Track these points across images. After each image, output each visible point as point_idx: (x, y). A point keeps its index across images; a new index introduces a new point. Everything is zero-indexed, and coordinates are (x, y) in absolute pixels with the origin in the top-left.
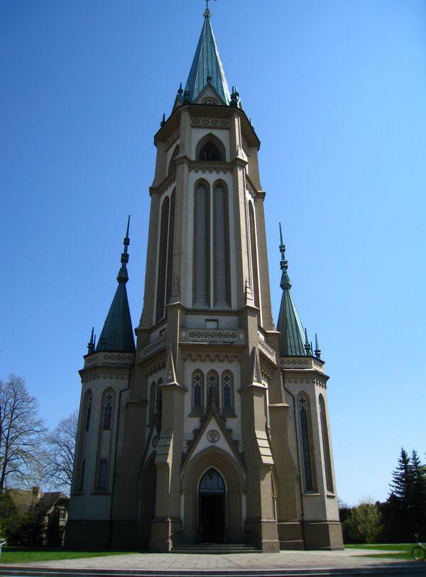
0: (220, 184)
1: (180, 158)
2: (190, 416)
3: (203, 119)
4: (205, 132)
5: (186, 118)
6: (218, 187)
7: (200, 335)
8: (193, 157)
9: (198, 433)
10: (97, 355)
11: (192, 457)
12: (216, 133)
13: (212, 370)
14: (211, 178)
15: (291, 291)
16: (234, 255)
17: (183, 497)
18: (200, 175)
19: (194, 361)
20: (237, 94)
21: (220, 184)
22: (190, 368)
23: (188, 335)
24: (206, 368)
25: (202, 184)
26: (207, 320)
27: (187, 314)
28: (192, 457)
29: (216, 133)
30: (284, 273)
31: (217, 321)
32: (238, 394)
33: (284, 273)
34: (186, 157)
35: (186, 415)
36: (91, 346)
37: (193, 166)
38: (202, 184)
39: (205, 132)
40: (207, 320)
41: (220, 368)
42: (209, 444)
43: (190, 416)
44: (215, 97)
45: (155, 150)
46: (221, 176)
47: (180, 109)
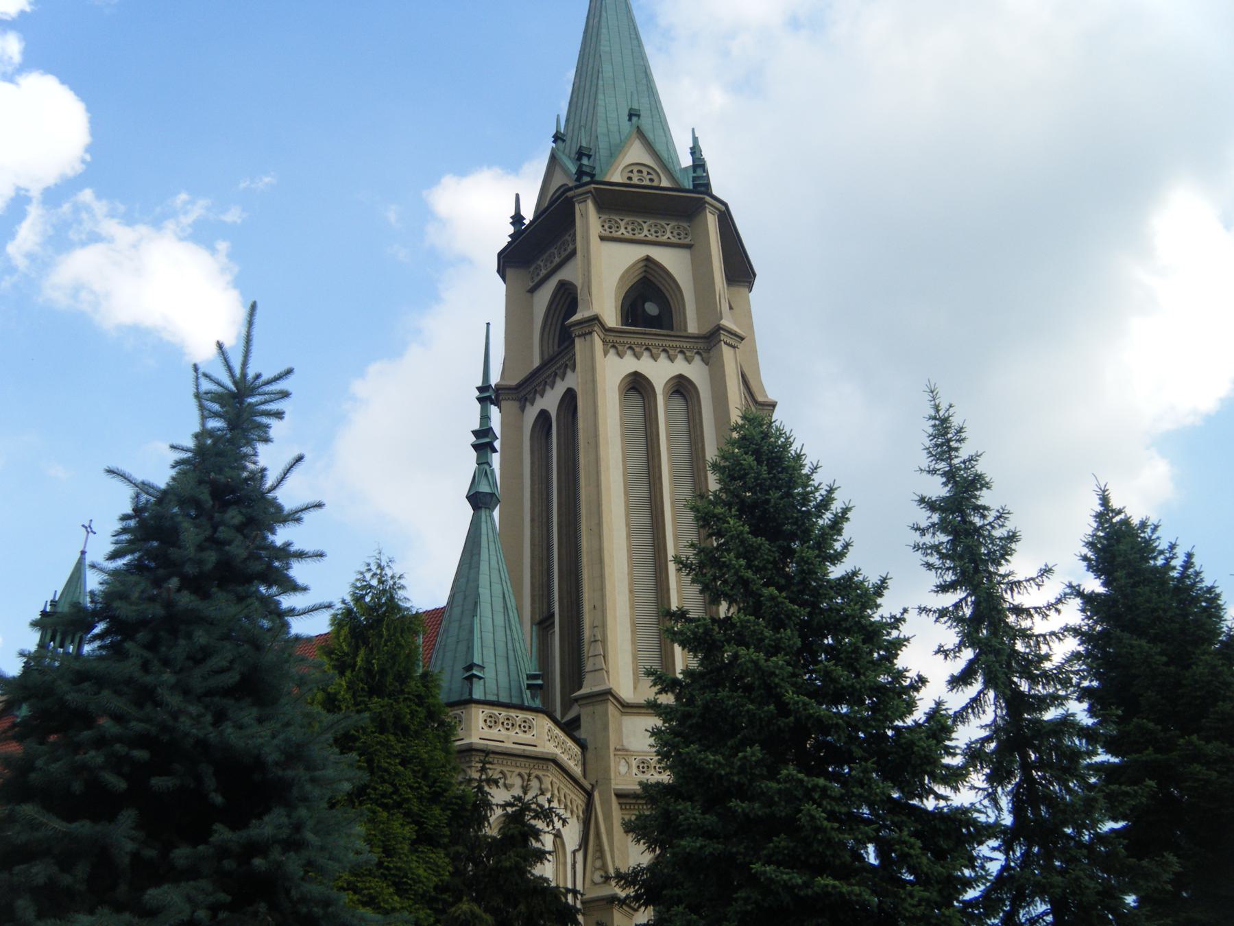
0: (681, 388)
1: (580, 323)
3: (627, 219)
5: (590, 220)
6: (631, 388)
8: (611, 318)
10: (529, 716)
12: (663, 256)
14: (660, 371)
16: (675, 578)
18: (629, 364)
20: (1070, 583)
21: (681, 388)
23: (635, 770)
25: (637, 385)
27: (623, 713)
29: (658, 254)
34: (596, 319)
37: (615, 342)
38: (637, 385)
45: (499, 287)
46: (680, 367)
47: (570, 194)
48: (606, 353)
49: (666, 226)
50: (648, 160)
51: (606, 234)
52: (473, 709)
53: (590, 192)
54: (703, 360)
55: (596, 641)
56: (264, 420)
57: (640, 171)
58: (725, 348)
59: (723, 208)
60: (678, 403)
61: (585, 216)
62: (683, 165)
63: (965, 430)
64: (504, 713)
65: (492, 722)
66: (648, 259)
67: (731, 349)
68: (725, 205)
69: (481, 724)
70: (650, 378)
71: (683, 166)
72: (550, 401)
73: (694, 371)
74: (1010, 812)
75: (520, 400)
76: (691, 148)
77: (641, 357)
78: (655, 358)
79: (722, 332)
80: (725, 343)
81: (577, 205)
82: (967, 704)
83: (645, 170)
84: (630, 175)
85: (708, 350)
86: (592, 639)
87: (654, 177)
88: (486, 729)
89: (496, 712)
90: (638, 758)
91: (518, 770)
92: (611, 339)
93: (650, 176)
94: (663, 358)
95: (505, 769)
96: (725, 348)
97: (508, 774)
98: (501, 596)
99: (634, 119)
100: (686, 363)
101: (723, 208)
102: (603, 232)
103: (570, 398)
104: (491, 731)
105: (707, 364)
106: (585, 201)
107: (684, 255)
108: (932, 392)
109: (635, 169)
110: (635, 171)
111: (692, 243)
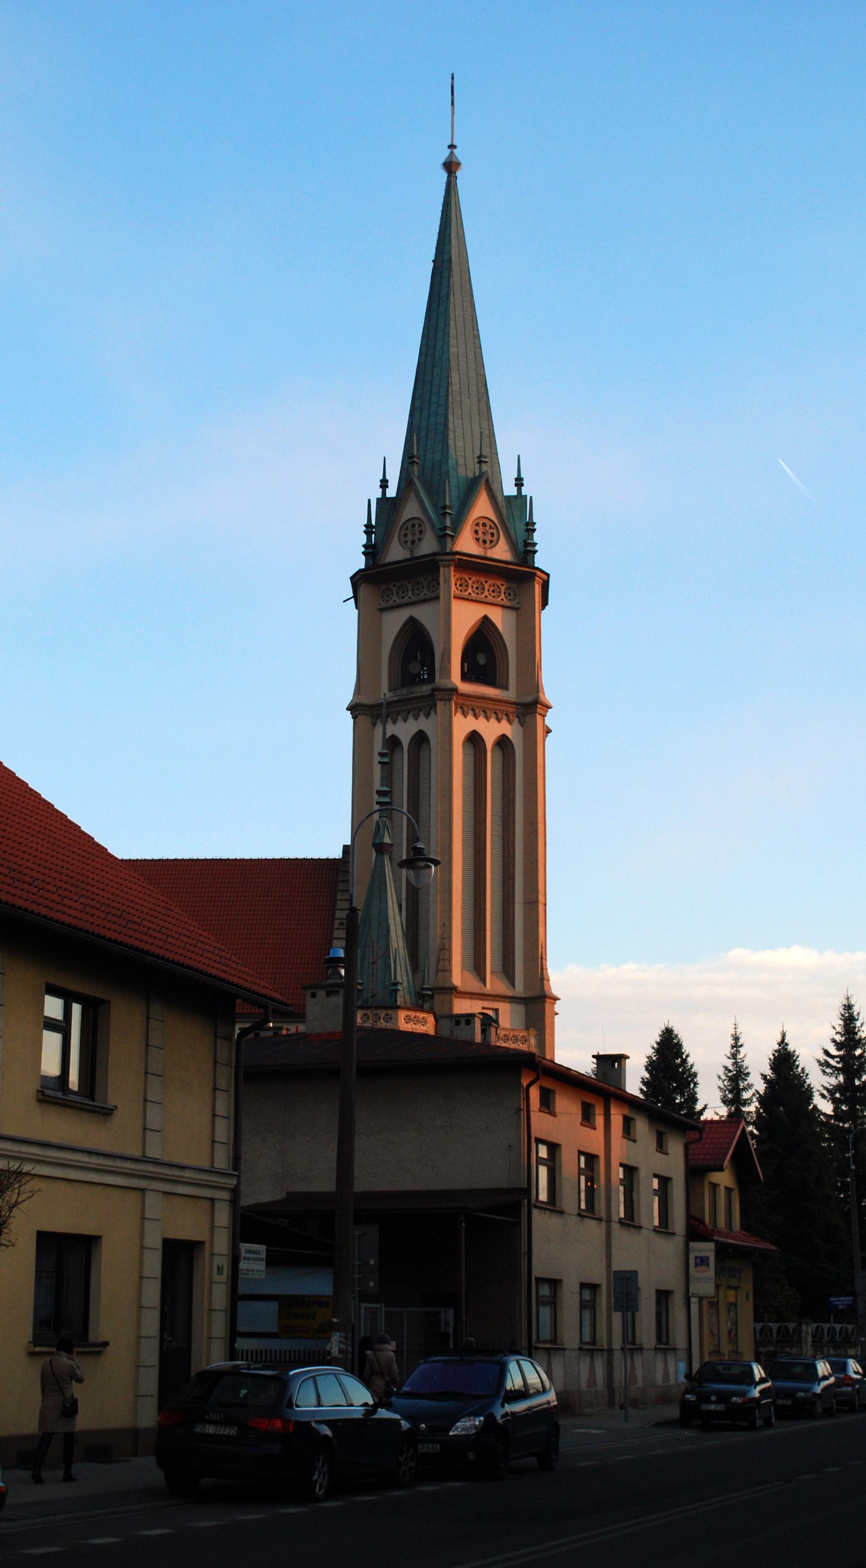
12: (497, 616)
15: (459, 174)
21: (503, 742)
38: (474, 739)
49: (501, 586)
50: (493, 517)
52: (399, 1013)
54: (520, 722)
55: (444, 949)
56: (599, 1120)
58: (538, 716)
61: (447, 581)
62: (506, 493)
64: (414, 1014)
65: (408, 1019)
66: (486, 619)
67: (541, 717)
68: (548, 575)
69: (403, 1020)
70: (483, 736)
71: (505, 494)
75: (372, 717)
76: (433, 261)
77: (479, 717)
78: (488, 718)
79: (539, 706)
80: (539, 714)
81: (442, 569)
83: (488, 523)
85: (525, 715)
86: (442, 947)
88: (405, 1024)
89: (410, 1014)
92: (461, 701)
93: (491, 531)
94: (493, 721)
96: (538, 716)
98: (400, 924)
100: (508, 724)
101: (545, 577)
103: (421, 738)
106: (449, 567)
107: (512, 614)
108: (735, 1025)
110: (480, 524)
111: (519, 606)
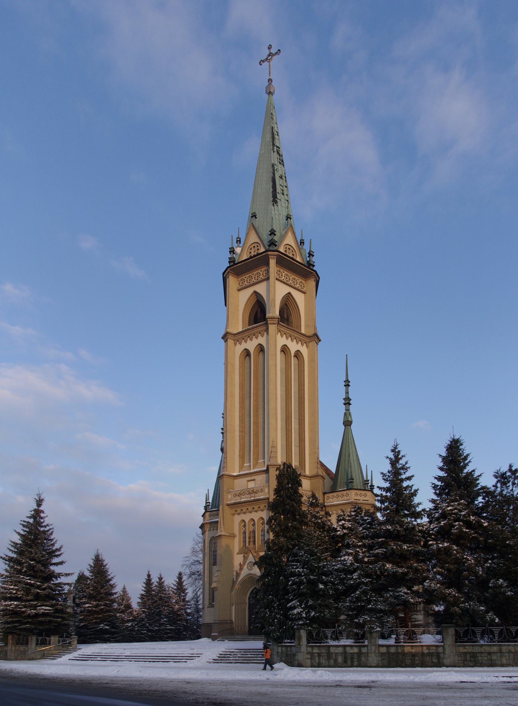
2: (238, 554)
4: (249, 292)
7: (240, 495)
9: (241, 566)
11: (238, 582)
13: (268, 80)
17: (234, 608)
18: (244, 345)
19: (239, 514)
21: (261, 349)
22: (237, 519)
24: (247, 517)
26: (248, 481)
27: (235, 479)
28: (238, 582)
30: (347, 410)
31: (254, 480)
32: (235, 533)
33: (347, 410)
35: (235, 553)
36: (206, 508)
38: (285, 350)
39: (249, 292)
40: (248, 481)
41: (256, 516)
42: (249, 572)
43: (238, 554)
44: (259, 242)
48: (235, 344)
51: (278, 277)
53: (229, 272)
57: (289, 249)
59: (318, 279)
60: (295, 358)
63: (402, 454)
66: (289, 293)
72: (251, 345)
73: (304, 350)
74: (44, 530)
75: (234, 340)
82: (384, 488)
83: (291, 249)
84: (286, 250)
87: (294, 254)
90: (232, 497)
91: (334, 509)
93: (293, 253)
95: (345, 508)
97: (346, 509)
99: (289, 219)
102: (239, 287)
104: (328, 501)
105: (307, 348)
109: (252, 246)
